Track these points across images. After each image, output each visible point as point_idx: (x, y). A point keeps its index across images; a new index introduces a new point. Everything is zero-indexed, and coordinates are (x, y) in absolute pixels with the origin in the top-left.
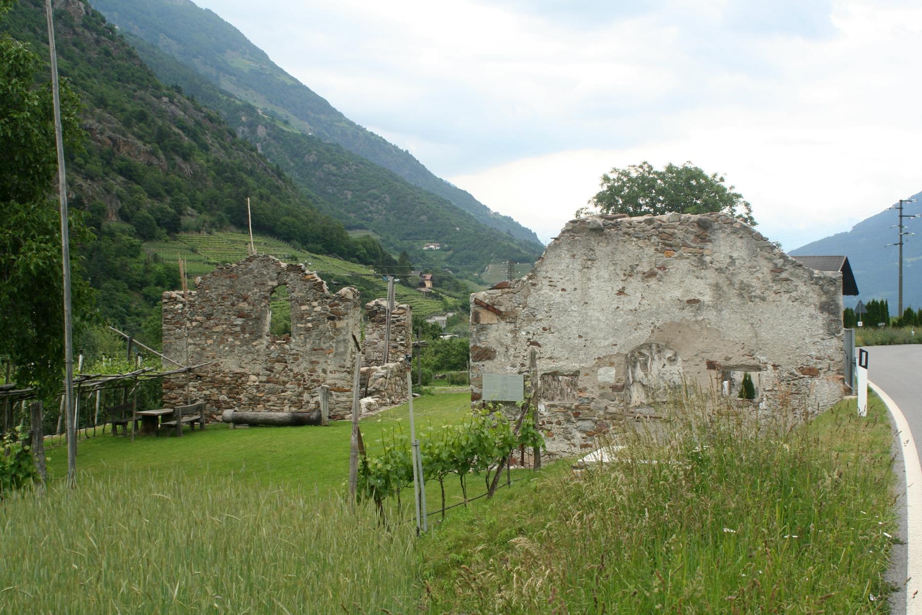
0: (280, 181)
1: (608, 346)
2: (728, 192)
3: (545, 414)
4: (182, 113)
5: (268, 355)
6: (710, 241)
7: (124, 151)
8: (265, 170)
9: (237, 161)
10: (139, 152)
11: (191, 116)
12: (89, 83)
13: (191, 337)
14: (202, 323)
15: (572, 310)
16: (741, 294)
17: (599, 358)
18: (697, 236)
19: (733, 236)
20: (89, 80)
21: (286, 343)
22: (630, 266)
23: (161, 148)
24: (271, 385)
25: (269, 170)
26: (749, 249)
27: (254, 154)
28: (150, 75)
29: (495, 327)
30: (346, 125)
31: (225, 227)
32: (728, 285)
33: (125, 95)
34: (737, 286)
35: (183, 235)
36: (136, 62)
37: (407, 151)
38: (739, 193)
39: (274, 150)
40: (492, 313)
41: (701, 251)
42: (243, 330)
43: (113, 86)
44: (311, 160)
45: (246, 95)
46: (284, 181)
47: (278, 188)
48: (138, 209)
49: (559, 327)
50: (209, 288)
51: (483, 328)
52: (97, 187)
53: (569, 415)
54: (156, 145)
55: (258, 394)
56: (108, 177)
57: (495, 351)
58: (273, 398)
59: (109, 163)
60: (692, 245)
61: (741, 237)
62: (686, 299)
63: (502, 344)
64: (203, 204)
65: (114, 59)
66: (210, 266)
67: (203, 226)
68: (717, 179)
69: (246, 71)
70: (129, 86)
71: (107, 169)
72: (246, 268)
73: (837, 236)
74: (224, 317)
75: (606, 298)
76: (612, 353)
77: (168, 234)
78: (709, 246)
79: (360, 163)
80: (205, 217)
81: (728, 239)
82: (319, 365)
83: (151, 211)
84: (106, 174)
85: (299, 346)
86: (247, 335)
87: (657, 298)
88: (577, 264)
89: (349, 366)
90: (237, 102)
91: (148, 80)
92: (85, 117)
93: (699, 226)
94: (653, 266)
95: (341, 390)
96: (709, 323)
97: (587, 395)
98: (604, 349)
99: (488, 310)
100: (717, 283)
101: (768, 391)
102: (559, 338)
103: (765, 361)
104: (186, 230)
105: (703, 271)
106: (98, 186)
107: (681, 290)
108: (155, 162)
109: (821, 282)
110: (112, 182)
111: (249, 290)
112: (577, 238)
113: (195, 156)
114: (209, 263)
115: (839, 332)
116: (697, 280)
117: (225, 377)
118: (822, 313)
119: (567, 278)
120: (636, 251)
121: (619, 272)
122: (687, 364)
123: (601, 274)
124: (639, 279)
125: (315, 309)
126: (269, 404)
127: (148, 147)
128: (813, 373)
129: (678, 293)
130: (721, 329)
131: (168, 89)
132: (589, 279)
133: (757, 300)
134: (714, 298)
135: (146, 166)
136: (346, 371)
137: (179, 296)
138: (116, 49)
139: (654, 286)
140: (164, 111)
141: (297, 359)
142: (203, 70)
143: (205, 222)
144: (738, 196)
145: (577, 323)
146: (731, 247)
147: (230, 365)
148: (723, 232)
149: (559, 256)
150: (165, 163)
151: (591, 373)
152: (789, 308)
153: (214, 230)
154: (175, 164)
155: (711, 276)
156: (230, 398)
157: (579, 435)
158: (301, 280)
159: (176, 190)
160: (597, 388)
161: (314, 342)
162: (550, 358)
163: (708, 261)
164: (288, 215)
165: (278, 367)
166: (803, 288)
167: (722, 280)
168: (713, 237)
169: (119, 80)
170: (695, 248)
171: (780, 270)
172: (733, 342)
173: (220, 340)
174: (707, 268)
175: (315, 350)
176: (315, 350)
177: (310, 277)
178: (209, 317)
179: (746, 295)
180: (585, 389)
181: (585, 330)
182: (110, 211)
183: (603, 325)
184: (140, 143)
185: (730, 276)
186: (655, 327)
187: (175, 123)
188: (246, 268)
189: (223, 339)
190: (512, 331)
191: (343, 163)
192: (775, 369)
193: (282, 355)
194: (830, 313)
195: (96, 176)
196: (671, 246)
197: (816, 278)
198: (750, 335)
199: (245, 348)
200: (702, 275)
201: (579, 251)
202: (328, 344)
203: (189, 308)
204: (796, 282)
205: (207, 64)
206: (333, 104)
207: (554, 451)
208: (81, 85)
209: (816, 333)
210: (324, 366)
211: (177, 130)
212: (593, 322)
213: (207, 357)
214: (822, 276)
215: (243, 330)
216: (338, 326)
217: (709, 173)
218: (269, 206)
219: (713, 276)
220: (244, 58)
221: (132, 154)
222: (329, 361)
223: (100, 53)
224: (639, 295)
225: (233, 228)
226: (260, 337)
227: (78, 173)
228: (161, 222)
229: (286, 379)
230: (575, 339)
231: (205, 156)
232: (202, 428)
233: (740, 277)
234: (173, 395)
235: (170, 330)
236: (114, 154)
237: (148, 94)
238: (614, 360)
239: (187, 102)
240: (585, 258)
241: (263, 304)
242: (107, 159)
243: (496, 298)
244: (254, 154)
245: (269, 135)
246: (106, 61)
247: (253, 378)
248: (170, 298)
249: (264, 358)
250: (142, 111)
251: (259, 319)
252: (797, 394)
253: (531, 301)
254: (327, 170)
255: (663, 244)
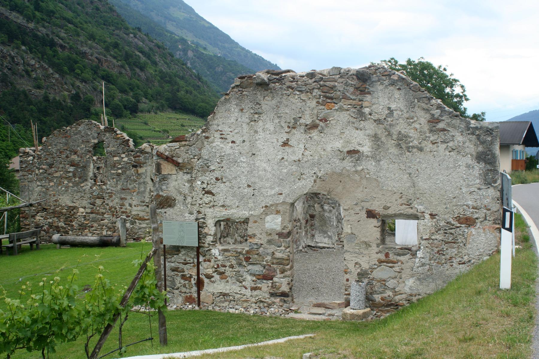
0: (200, 83)
1: (274, 195)
2: (449, 77)
3: (220, 258)
4: (142, 43)
5: (92, 193)
6: (369, 93)
7: (105, 66)
8: (191, 76)
9: (174, 71)
10: (114, 66)
11: (147, 45)
12: (85, 26)
13: (39, 181)
14: (46, 170)
15: (241, 161)
16: (399, 145)
17: (266, 207)
18: (357, 89)
19: (391, 88)
20: (85, 24)
21: (104, 185)
22: (294, 119)
23: (127, 64)
24: (94, 215)
25: (193, 76)
26: (407, 101)
27: (184, 67)
28: (123, 22)
29: (174, 177)
30: (240, 50)
31: (165, 109)
32: (386, 136)
33: (108, 33)
34: (395, 137)
35: (140, 114)
36: (115, 14)
37: (276, 65)
38: (457, 79)
39: (198, 65)
40: (171, 164)
41: (360, 103)
42: (74, 176)
43: (101, 28)
44: (220, 70)
45: (182, 33)
46: (202, 82)
47: (198, 86)
48: (113, 99)
49: (230, 177)
50: (51, 145)
51: (164, 179)
52: (89, 87)
53: (240, 260)
54: (124, 62)
55: (85, 222)
56: (96, 80)
57: (175, 200)
58: (95, 225)
59: (96, 73)
60: (351, 97)
61: (399, 89)
62: (346, 150)
63: (180, 193)
64: (152, 96)
65: (101, 12)
66: (155, 133)
67: (152, 109)
68: (442, 69)
69: (181, 19)
70: (110, 28)
71: (95, 76)
72: (76, 130)
73: (530, 112)
74: (61, 166)
75: (272, 149)
76: (278, 202)
77: (131, 114)
78: (368, 97)
79: (248, 72)
80: (154, 104)
81: (386, 90)
82: (126, 201)
83: (121, 101)
84: (94, 79)
85: (112, 187)
86: (77, 179)
87: (319, 149)
88: (245, 118)
89: (147, 201)
90: (176, 37)
91: (121, 24)
92: (82, 46)
93: (358, 78)
94: (315, 118)
95: (142, 219)
96: (368, 173)
97: (256, 241)
98: (270, 198)
99: (168, 161)
100: (376, 134)
101: (426, 239)
102: (230, 187)
103: (423, 210)
104: (142, 111)
105: (362, 122)
106: (89, 86)
107: (341, 141)
108: (123, 71)
109: (477, 132)
110: (97, 84)
111: (78, 146)
112: (244, 93)
113: (148, 68)
114: (155, 131)
115: (495, 182)
116: (357, 131)
117: (62, 209)
118: (478, 163)
119: (236, 131)
120: (299, 104)
121: (283, 125)
122: (347, 213)
123: (267, 126)
124: (302, 131)
125: (124, 160)
126: (93, 229)
127: (120, 63)
128: (469, 222)
129: (338, 144)
130: (379, 179)
131: (133, 29)
132: (256, 132)
133: (415, 150)
134: (373, 148)
135: (118, 75)
136: (145, 205)
137: (31, 151)
138: (103, 6)
139: (315, 137)
140: (131, 42)
141: (111, 197)
142: (156, 19)
143: (153, 106)
144: (456, 81)
145: (246, 173)
146: (389, 98)
147: (66, 200)
148: (382, 84)
149: (229, 110)
150: (129, 72)
151: (259, 221)
152: (446, 158)
153: (158, 112)
154: (136, 73)
155: (370, 127)
156: (66, 224)
157: (249, 278)
158: (114, 138)
159: (136, 88)
160: (264, 235)
161: (123, 184)
162: (223, 206)
163: (367, 113)
164: (203, 102)
165: (99, 202)
166: (459, 138)
167: (380, 131)
168: (371, 89)
169: (104, 25)
170: (354, 100)
171: (437, 121)
172: (391, 191)
173: (58, 182)
174: (366, 119)
175: (124, 190)
176: (124, 190)
177: (120, 136)
178: (51, 166)
179: (404, 146)
180: (254, 235)
181: (253, 180)
182: (96, 101)
183: (269, 175)
184: (114, 61)
185: (388, 127)
186: (317, 177)
187: (137, 49)
188: (76, 130)
189: (60, 182)
190: (189, 181)
191: (238, 72)
192: (432, 218)
193: (101, 193)
194: (486, 163)
195: (88, 80)
196: (332, 98)
197: (472, 128)
198: (408, 185)
199: (75, 188)
200: (361, 126)
201: (247, 105)
202: (132, 186)
203: (38, 159)
204: (453, 132)
205: (159, 15)
206: (233, 37)
207: (227, 292)
208: (80, 27)
209: (473, 182)
210: (130, 201)
211: (138, 53)
212: (260, 172)
213: (50, 195)
214: (479, 126)
215: (74, 176)
216: (139, 172)
217: (436, 65)
218: (192, 97)
219: (372, 127)
220: (180, 11)
221: (110, 67)
222: (133, 198)
223: (93, 9)
224: (302, 146)
225: (170, 110)
226: (86, 180)
227: (77, 79)
228: (127, 107)
229: (104, 211)
230: (244, 189)
231: (154, 68)
232: (38, 248)
233: (398, 128)
234: (27, 222)
235: (25, 176)
236: (99, 67)
237: (121, 32)
238: (280, 208)
239: (144, 37)
240: (252, 111)
241: (88, 156)
242: (95, 71)
243: (174, 151)
244: (184, 67)
245: (195, 56)
246: (96, 14)
247: (81, 210)
248: (24, 153)
249: (89, 195)
250: (116, 42)
251: (85, 167)
252: (454, 243)
253: (205, 153)
254: (228, 76)
255: (324, 96)
